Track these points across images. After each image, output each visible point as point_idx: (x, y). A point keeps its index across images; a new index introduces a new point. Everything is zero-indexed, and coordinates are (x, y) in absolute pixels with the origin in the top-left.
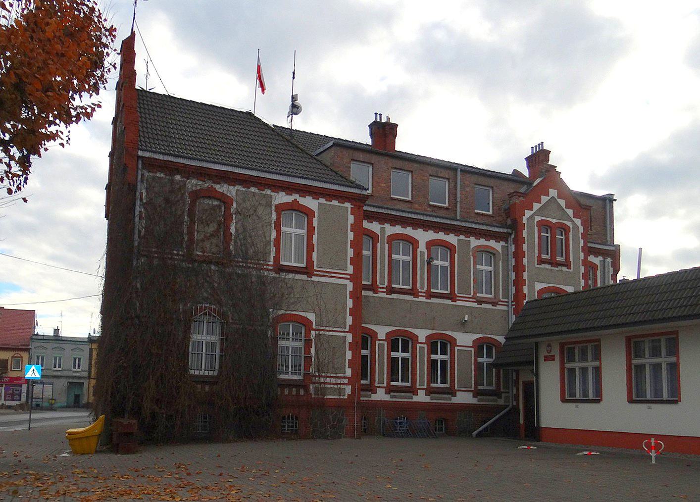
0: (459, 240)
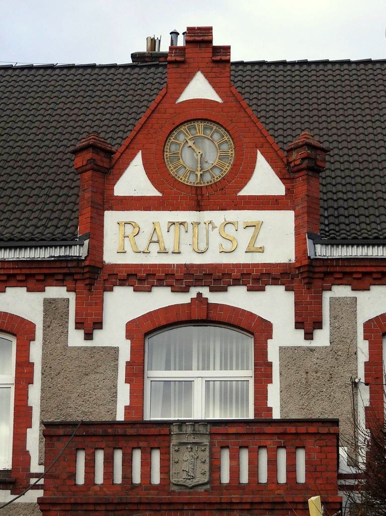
0: (49, 304)
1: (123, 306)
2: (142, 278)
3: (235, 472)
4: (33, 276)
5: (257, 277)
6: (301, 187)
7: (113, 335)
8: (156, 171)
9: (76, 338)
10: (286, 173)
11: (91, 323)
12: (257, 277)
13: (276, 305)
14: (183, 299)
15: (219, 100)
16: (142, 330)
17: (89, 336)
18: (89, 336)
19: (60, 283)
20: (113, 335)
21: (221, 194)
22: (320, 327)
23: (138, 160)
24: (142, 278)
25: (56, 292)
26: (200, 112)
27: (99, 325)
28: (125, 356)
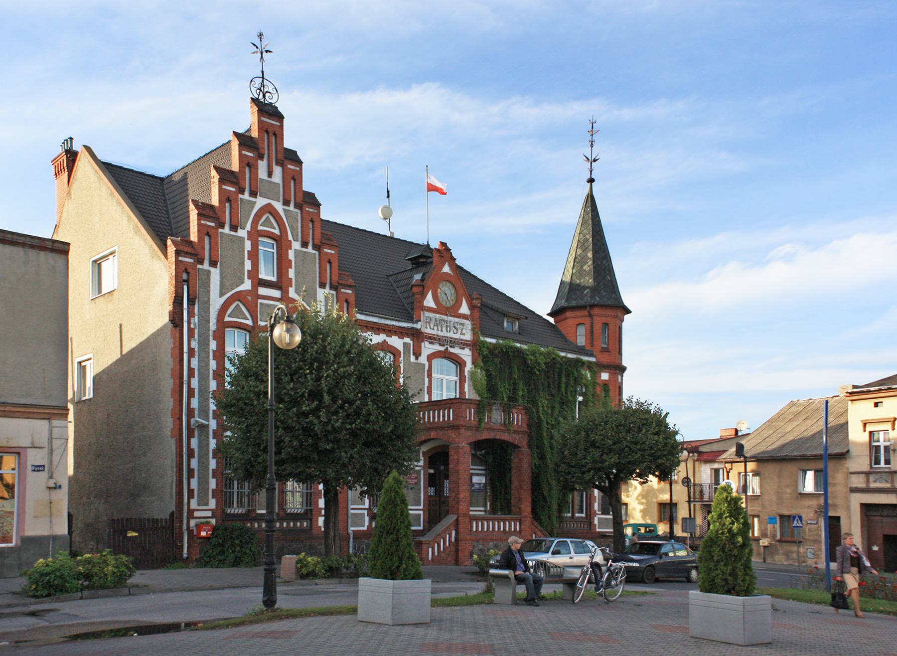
0: (405, 344)
1: (428, 348)
2: (432, 339)
3: (515, 525)
4: (401, 333)
5: (463, 344)
6: (477, 314)
7: (423, 359)
8: (436, 298)
9: (413, 359)
10: (472, 307)
11: (417, 355)
12: (463, 344)
13: (466, 354)
14: (442, 349)
15: (430, 293)
16: (430, 358)
17: (417, 358)
18: (417, 358)
19: (408, 337)
20: (423, 359)
21: (452, 311)
22: (683, 519)
23: (430, 293)
24: (432, 339)
25: (407, 340)
26: (446, 278)
27: (420, 355)
28: (427, 368)
